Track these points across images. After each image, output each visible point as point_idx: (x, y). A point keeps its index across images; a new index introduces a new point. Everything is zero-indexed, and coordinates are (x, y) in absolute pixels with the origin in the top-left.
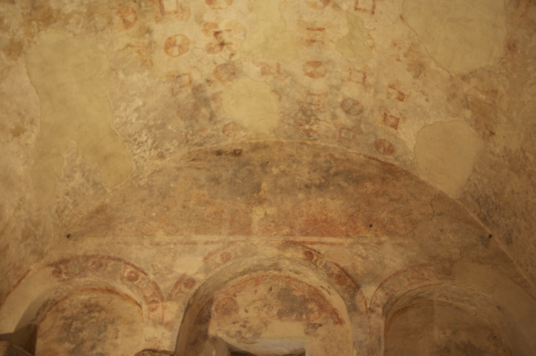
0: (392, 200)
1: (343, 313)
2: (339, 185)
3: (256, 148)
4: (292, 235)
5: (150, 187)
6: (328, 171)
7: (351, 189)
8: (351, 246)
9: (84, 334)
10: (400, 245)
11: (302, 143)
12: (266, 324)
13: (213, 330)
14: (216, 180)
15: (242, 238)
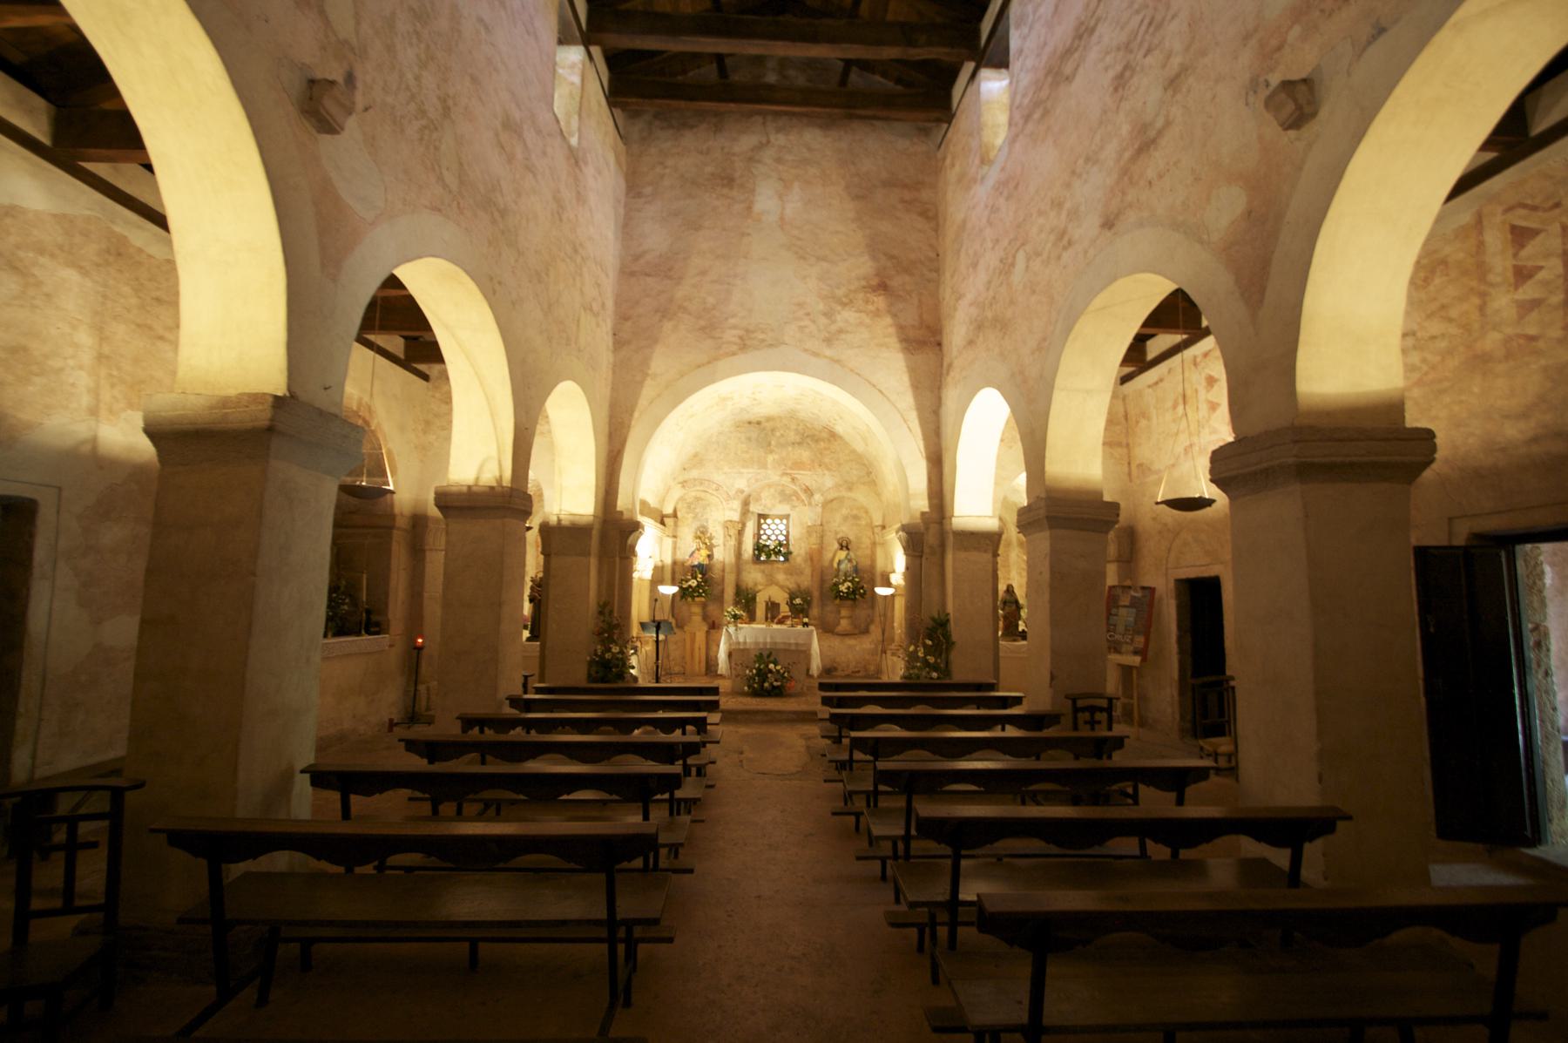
0: (832, 452)
1: (806, 502)
3: (769, 419)
7: (813, 446)
9: (697, 511)
10: (833, 476)
14: (749, 439)
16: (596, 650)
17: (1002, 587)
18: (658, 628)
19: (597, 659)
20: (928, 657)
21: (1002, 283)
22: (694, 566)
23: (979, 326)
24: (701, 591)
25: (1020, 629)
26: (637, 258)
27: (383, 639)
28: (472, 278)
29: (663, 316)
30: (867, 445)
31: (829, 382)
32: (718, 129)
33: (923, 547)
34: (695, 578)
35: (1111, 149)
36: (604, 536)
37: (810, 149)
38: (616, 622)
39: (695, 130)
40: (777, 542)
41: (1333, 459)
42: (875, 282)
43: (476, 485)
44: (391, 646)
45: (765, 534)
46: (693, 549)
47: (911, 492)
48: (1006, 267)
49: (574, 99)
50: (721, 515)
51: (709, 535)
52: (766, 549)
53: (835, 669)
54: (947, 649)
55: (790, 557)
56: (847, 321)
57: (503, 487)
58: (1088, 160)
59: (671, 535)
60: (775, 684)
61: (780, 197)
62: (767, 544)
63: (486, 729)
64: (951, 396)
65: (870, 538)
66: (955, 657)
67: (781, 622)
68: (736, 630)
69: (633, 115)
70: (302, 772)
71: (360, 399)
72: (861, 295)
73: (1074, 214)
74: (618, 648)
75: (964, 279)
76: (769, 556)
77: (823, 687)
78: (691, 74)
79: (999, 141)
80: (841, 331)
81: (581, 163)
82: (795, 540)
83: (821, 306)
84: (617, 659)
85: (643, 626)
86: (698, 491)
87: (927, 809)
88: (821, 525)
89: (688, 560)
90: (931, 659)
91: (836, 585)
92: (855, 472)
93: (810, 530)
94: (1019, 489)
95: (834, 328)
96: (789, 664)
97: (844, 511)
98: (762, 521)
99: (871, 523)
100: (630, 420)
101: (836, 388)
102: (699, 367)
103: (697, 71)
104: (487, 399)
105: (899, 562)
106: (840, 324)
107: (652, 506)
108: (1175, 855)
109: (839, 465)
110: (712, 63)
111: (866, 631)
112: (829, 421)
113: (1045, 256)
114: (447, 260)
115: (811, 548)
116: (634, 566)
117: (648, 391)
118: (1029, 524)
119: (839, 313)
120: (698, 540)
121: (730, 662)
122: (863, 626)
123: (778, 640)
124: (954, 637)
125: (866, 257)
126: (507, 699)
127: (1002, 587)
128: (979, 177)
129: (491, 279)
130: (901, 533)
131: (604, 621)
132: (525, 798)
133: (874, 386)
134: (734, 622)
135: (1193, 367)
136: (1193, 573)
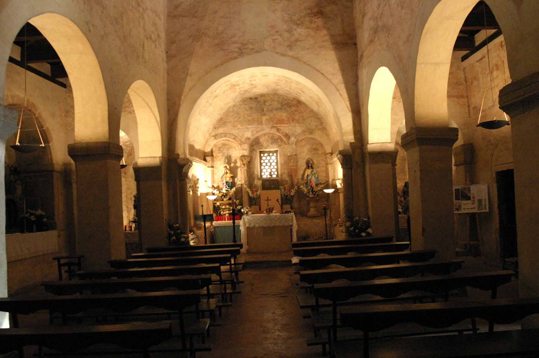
2: (285, 108)
3: (262, 95)
7: (288, 110)
8: (288, 126)
9: (224, 151)
10: (301, 126)
14: (251, 108)
15: (260, 126)
26: (176, 7)
30: (319, 107)
36: (169, 169)
42: (315, 10)
45: (264, 162)
47: (343, 131)
56: (300, 34)
64: (363, 73)
71: (28, 100)
72: (308, 19)
80: (297, 40)
83: (285, 27)
86: (223, 140)
92: (313, 123)
95: (293, 39)
98: (262, 155)
99: (325, 152)
102: (216, 67)
105: (339, 172)
108: (491, 328)
112: (297, 94)
117: (189, 83)
118: (408, 143)
130: (339, 156)
133: (319, 71)
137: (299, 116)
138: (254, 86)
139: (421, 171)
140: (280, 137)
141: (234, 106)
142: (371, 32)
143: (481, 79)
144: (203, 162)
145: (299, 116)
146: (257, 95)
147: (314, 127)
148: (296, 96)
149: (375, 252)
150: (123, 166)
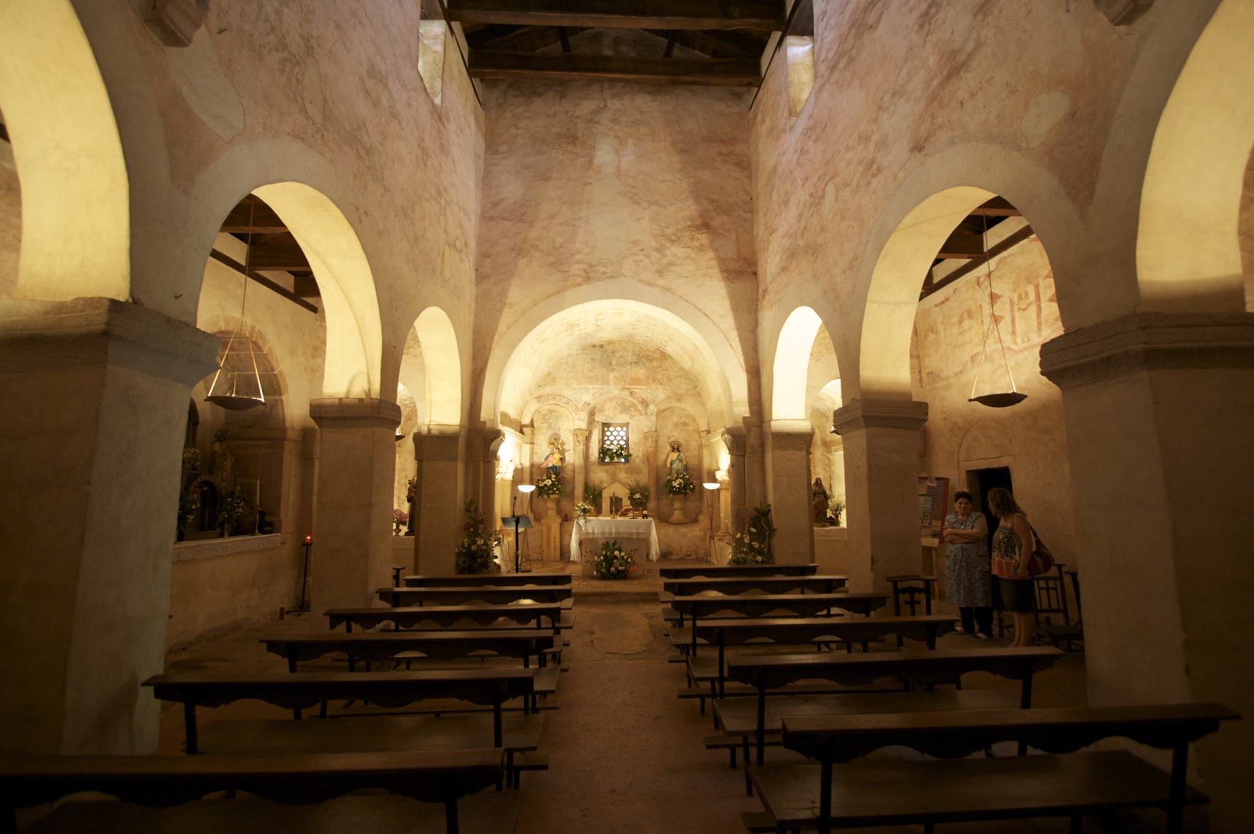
0: (663, 370)
2: (643, 362)
3: (610, 343)
4: (624, 385)
5: (567, 363)
6: (639, 356)
7: (648, 364)
8: (647, 389)
9: (551, 421)
10: (665, 389)
11: (629, 341)
12: (615, 416)
13: (597, 418)
14: (594, 360)
15: (606, 386)
16: (463, 543)
17: (813, 482)
18: (517, 522)
19: (464, 551)
20: (753, 543)
21: (812, 215)
22: (548, 468)
23: (792, 254)
24: (555, 489)
25: (828, 515)
26: (495, 205)
27: (275, 537)
28: (338, 206)
29: (519, 254)
30: (693, 363)
31: (662, 308)
32: (563, 96)
33: (745, 447)
34: (550, 478)
35: (919, 79)
36: (469, 444)
37: (641, 112)
38: (481, 518)
39: (543, 97)
40: (619, 446)
41: (1182, 345)
42: (698, 222)
43: (347, 398)
44: (283, 543)
46: (548, 454)
48: (817, 199)
49: (437, 65)
50: (571, 424)
51: (561, 441)
52: (610, 453)
53: (671, 553)
54: (769, 536)
55: (631, 459)
56: (675, 255)
57: (372, 399)
58: (894, 94)
59: (529, 442)
60: (620, 568)
61: (617, 152)
62: (610, 448)
63: (353, 624)
64: (767, 317)
65: (697, 441)
66: (777, 542)
67: (624, 514)
68: (586, 522)
69: (490, 84)
70: (145, 684)
71: (253, 328)
72: (687, 234)
73: (883, 144)
74: (482, 540)
75: (777, 215)
76: (612, 458)
77: (664, 573)
78: (538, 51)
79: (804, 97)
80: (671, 264)
81: (444, 120)
82: (634, 444)
84: (482, 550)
85: (504, 520)
86: (551, 404)
87: (734, 656)
88: (656, 431)
89: (544, 463)
90: (756, 544)
91: (670, 481)
92: (683, 386)
93: (646, 436)
94: (833, 394)
95: (664, 261)
96: (631, 551)
97: (675, 419)
98: (606, 429)
100: (491, 344)
101: (668, 313)
102: (550, 296)
103: (544, 48)
104: (357, 320)
105: (724, 460)
106: (670, 258)
107: (512, 417)
109: (671, 380)
110: (557, 41)
111: (696, 521)
112: (661, 343)
113: (854, 184)
114: (311, 186)
115: (647, 451)
116: (497, 469)
117: (506, 317)
119: (669, 248)
120: (552, 446)
121: (580, 549)
122: (693, 516)
123: (622, 530)
124: (775, 526)
125: (690, 202)
126: (377, 592)
127: (813, 482)
128: (788, 127)
129: (358, 209)
130: (726, 436)
131: (470, 517)
132: (424, 655)
133: (700, 310)
134: (584, 515)
135: (977, 287)
136: (983, 465)
137: (663, 375)
138: (599, 328)
139: (869, 466)
140: (634, 403)
141: (569, 355)
142: (784, 256)
143: (942, 331)
144: (518, 434)
145: (663, 375)
146: (604, 341)
147: (684, 392)
148: (659, 345)
149: (790, 590)
150: (399, 438)
